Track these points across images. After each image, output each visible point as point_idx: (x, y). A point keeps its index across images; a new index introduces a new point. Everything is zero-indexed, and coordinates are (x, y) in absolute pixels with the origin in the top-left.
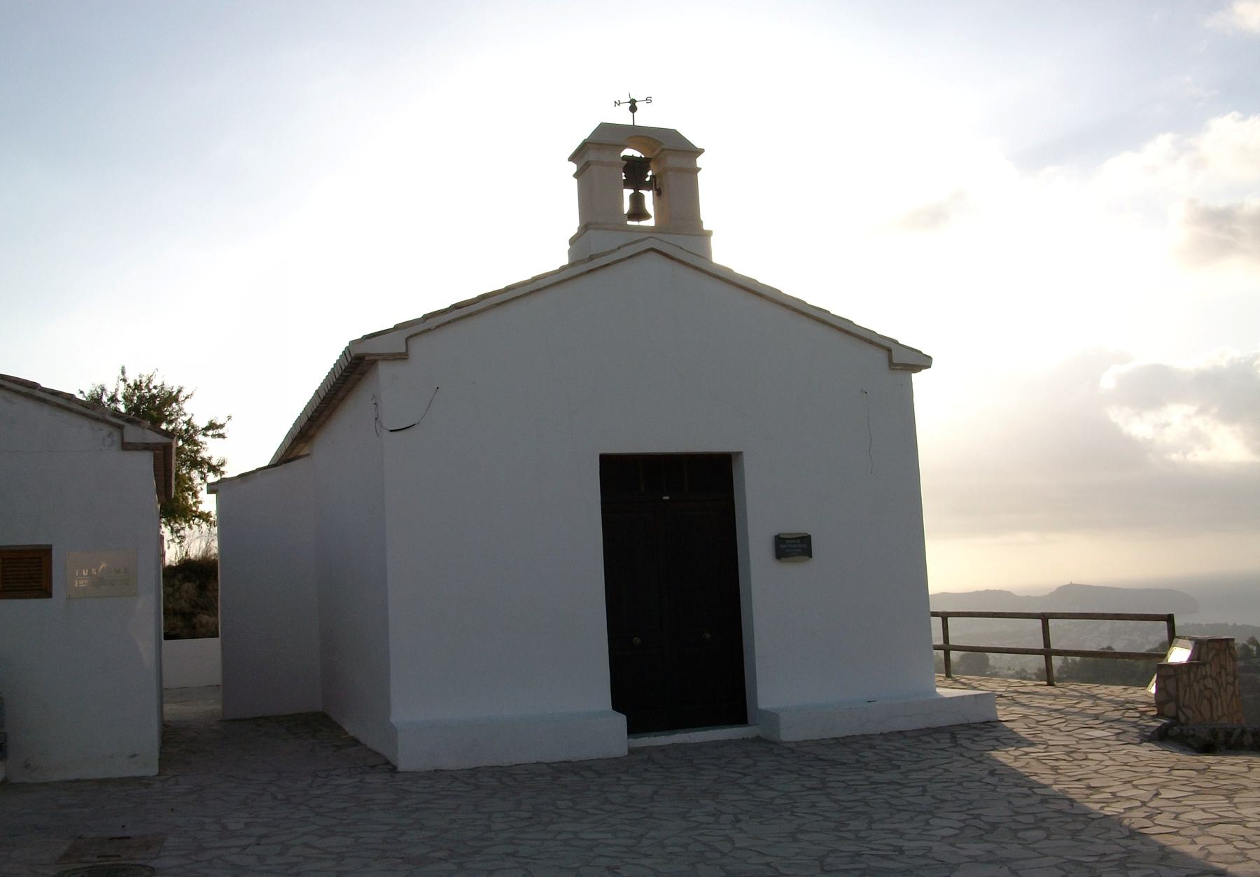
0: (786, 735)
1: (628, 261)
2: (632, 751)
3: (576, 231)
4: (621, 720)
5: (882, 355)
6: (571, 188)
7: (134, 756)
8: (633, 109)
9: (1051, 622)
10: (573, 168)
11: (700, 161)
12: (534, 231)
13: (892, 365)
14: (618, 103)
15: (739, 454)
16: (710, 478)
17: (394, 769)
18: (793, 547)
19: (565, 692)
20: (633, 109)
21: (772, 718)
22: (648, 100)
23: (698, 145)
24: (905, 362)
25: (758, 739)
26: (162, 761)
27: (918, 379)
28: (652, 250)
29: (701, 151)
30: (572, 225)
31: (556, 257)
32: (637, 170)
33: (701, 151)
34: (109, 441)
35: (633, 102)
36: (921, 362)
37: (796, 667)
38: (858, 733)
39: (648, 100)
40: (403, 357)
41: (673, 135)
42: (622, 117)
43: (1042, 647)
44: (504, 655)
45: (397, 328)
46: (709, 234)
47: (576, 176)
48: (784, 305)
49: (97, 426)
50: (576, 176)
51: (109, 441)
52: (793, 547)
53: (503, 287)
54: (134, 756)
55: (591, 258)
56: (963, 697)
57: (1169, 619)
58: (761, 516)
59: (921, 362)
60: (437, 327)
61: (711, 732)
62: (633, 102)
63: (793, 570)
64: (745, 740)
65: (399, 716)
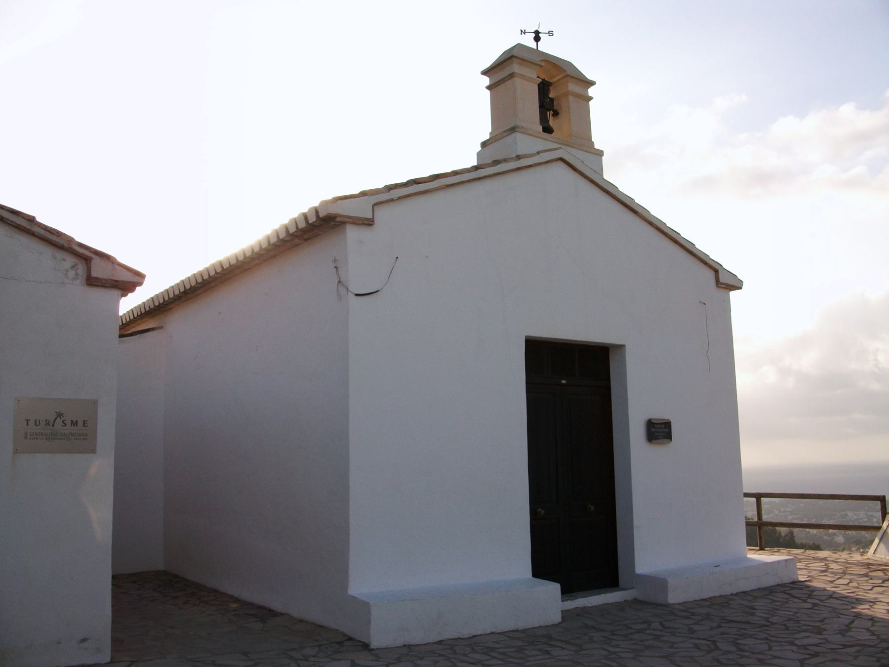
0: (674, 597)
1: (544, 166)
2: (566, 614)
4: (555, 588)
5: (711, 275)
7: (84, 640)
8: (537, 39)
9: (764, 500)
10: (486, 81)
12: (455, 130)
14: (523, 32)
15: (621, 347)
16: (668, 436)
17: (366, 646)
18: (658, 431)
20: (537, 39)
21: (659, 583)
22: (550, 33)
23: (590, 77)
24: (725, 283)
25: (636, 601)
26: (117, 643)
27: (733, 294)
28: (562, 159)
29: (591, 83)
30: (485, 131)
31: (466, 158)
33: (591, 83)
34: (72, 274)
35: (537, 33)
36: (735, 285)
37: (670, 537)
38: (717, 594)
39: (550, 33)
40: (368, 223)
43: (756, 519)
44: (437, 524)
45: (364, 194)
46: (600, 153)
47: (488, 88)
48: (651, 224)
49: (61, 255)
50: (488, 88)
51: (72, 274)
52: (658, 431)
53: (449, 171)
54: (84, 640)
55: (496, 163)
56: (779, 562)
57: (882, 499)
59: (735, 285)
60: (399, 198)
61: (608, 595)
62: (537, 33)
63: (659, 451)
64: (617, 604)
65: (360, 585)
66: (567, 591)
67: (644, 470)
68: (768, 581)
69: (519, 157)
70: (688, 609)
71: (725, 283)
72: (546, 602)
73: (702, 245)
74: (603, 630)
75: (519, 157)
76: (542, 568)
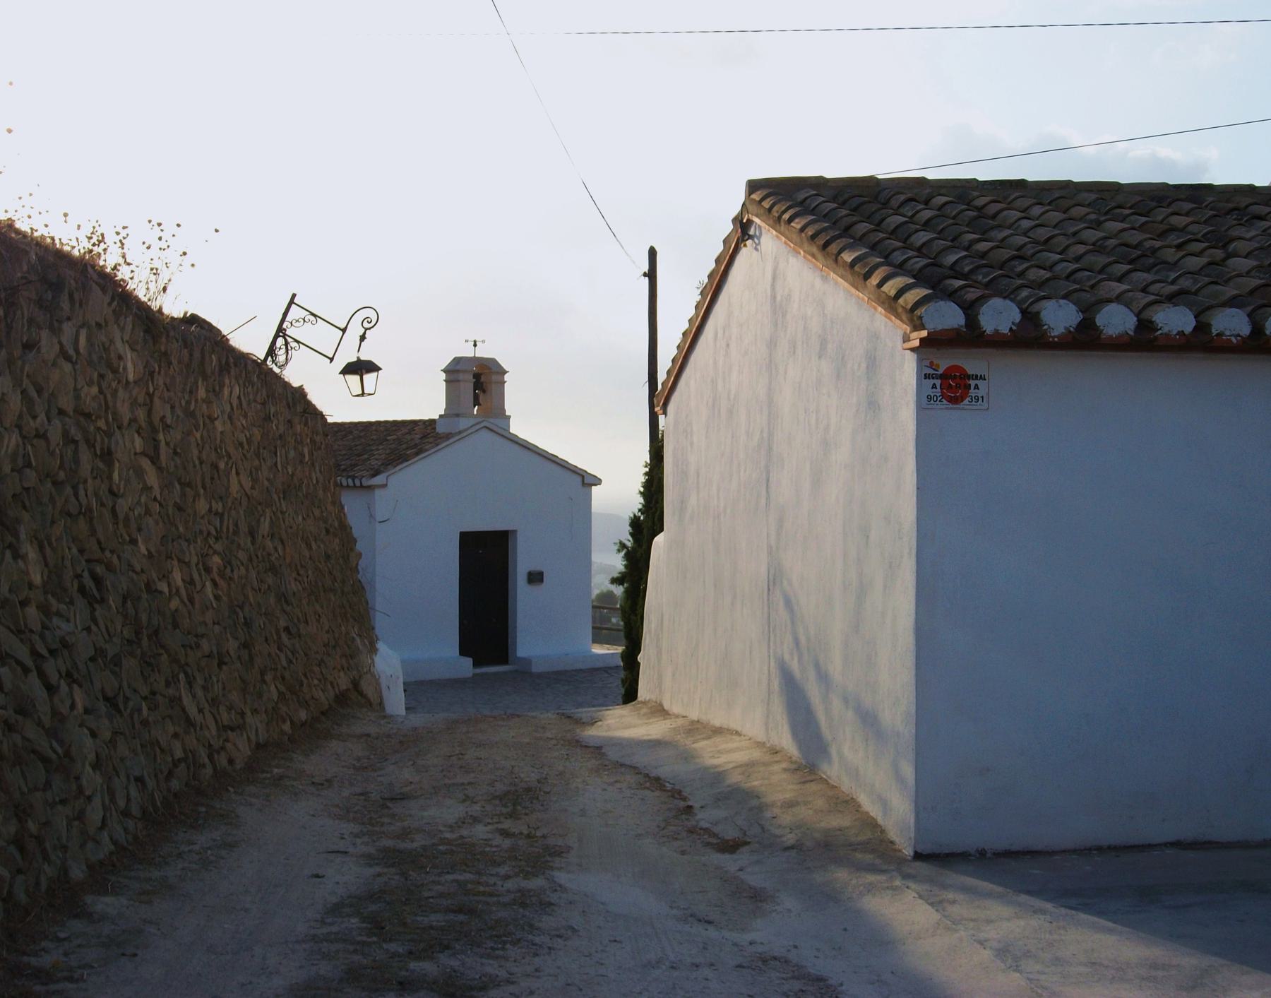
0: (534, 670)
3: (639, 658)
4: (469, 661)
5: (579, 479)
6: (443, 386)
11: (506, 377)
13: (584, 484)
15: (514, 532)
16: (541, 580)
19: (441, 649)
21: (527, 661)
22: (483, 342)
32: (477, 381)
36: (598, 481)
39: (483, 342)
41: (494, 361)
42: (469, 353)
52: (535, 578)
58: (523, 562)
59: (598, 481)
61: (1110, 939)
63: (535, 590)
64: (505, 673)
66: (476, 664)
67: (524, 598)
68: (599, 664)
69: (460, 432)
70: (540, 675)
71: (587, 481)
72: (466, 666)
73: (573, 461)
74: (202, 353)
75: (460, 432)
76: (464, 651)
